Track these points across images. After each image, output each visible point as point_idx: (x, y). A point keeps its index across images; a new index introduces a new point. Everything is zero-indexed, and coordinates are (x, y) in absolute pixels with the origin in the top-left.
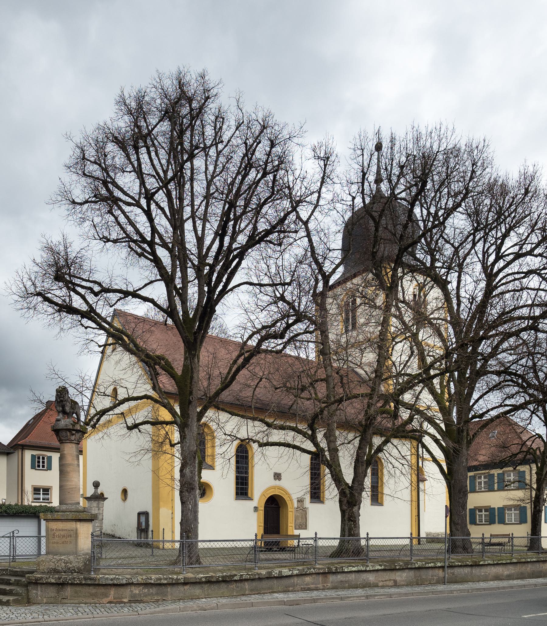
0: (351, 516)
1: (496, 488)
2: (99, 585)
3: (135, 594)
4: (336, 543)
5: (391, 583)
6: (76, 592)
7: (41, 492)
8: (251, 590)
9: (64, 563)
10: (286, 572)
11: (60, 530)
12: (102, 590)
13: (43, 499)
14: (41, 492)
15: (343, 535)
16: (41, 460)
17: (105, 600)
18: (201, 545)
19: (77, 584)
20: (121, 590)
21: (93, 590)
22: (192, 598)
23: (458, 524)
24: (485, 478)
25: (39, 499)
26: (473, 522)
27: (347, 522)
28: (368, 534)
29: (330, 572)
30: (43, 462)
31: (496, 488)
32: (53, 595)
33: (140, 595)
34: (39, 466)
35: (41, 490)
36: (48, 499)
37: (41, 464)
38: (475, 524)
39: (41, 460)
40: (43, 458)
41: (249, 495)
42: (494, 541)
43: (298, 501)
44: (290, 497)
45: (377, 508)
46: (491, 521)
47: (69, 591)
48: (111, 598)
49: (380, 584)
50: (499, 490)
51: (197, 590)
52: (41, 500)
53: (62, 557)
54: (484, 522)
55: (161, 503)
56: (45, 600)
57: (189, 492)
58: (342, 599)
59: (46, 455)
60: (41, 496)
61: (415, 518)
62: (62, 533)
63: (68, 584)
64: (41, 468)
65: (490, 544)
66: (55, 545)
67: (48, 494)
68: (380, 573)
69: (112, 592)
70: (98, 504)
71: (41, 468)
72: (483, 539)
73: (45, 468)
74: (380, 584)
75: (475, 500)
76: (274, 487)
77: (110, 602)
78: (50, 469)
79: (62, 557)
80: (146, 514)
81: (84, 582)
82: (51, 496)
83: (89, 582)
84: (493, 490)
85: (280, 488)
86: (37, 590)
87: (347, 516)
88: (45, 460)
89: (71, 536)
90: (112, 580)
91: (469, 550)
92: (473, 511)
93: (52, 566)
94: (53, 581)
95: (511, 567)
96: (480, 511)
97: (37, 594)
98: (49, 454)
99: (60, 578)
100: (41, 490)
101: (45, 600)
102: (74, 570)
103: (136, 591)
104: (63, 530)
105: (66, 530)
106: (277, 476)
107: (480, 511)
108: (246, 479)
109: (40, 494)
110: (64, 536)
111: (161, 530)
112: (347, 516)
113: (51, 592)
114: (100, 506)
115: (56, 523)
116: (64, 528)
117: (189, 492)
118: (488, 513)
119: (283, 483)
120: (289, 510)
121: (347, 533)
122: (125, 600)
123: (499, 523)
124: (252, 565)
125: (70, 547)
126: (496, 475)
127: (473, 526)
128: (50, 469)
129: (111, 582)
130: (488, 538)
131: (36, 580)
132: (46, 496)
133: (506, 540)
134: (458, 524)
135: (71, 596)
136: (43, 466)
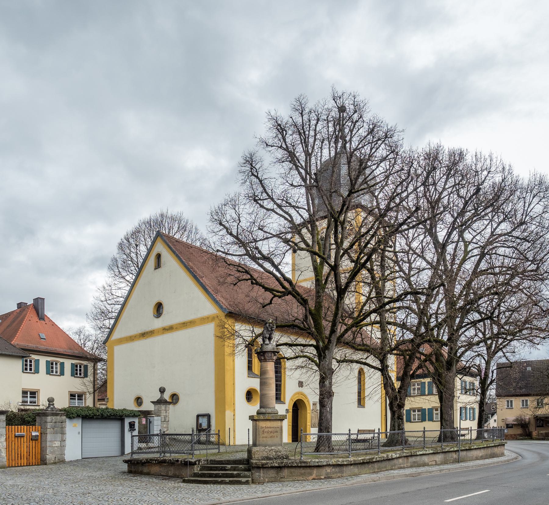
0: (400, 416)
1: (427, 393)
2: (310, 467)
3: (328, 473)
4: (439, 433)
5: (434, 463)
6: (291, 473)
7: (29, 395)
8: (378, 469)
9: (275, 452)
10: (394, 456)
11: (268, 428)
12: (308, 470)
13: (31, 402)
14: (29, 395)
15: (441, 429)
16: (78, 368)
17: (311, 478)
18: (334, 438)
19: (295, 467)
20: (320, 470)
21: (302, 471)
22: (356, 475)
23: (447, 421)
24: (418, 385)
25: (27, 402)
26: (409, 420)
27: (396, 420)
28: (350, 430)
29: (411, 456)
30: (80, 370)
31: (427, 393)
32: (273, 475)
33: (330, 473)
34: (77, 374)
35: (29, 393)
36: (35, 402)
37: (78, 372)
38: (410, 422)
39: (78, 368)
40: (80, 367)
41: (282, 400)
42: (361, 437)
43: (313, 404)
44: (308, 401)
45: (361, 409)
46: (423, 420)
47: (286, 472)
48: (314, 476)
49: (430, 464)
50: (428, 395)
51: (355, 470)
52: (29, 403)
53: (273, 448)
54: (417, 420)
55: (227, 407)
56: (267, 480)
57: (328, 399)
58: (430, 472)
59: (58, 362)
60: (29, 399)
61: (384, 417)
62: (270, 430)
63: (285, 467)
64: (78, 375)
65: (358, 441)
66: (264, 439)
67: (35, 397)
68: (430, 456)
69: (315, 471)
70: (166, 407)
71: (28, 371)
72: (349, 435)
73: (32, 372)
74: (430, 464)
75: (409, 404)
76: (298, 393)
77: (314, 479)
78: (38, 372)
79: (273, 448)
80: (208, 416)
81: (300, 465)
82: (38, 400)
83: (303, 465)
84: (424, 395)
85: (302, 394)
86: (260, 473)
87: (396, 415)
88: (82, 369)
89: (277, 432)
90: (318, 462)
91: (455, 440)
92: (408, 412)
93: (265, 454)
94: (276, 465)
95: (482, 450)
96: (414, 411)
97: (259, 476)
98: (62, 360)
99: (282, 463)
100: (29, 393)
101: (267, 480)
102: (283, 457)
103: (329, 470)
104: (270, 428)
105: (273, 427)
106: (301, 384)
107: (414, 411)
108: (280, 385)
109: (75, 399)
110: (271, 432)
111: (227, 429)
112: (396, 415)
113: (272, 473)
114: (167, 409)
115: (265, 422)
116: (272, 426)
117: (328, 399)
118: (420, 413)
119: (305, 390)
120: (308, 411)
121: (397, 428)
122: (323, 477)
123: (429, 420)
124: (346, 454)
125: (276, 440)
126: (427, 384)
127: (409, 423)
128: (38, 372)
129: (317, 464)
130: (354, 434)
131: (263, 465)
132: (33, 399)
133: (466, 432)
134: (447, 421)
135: (287, 476)
136: (31, 369)
